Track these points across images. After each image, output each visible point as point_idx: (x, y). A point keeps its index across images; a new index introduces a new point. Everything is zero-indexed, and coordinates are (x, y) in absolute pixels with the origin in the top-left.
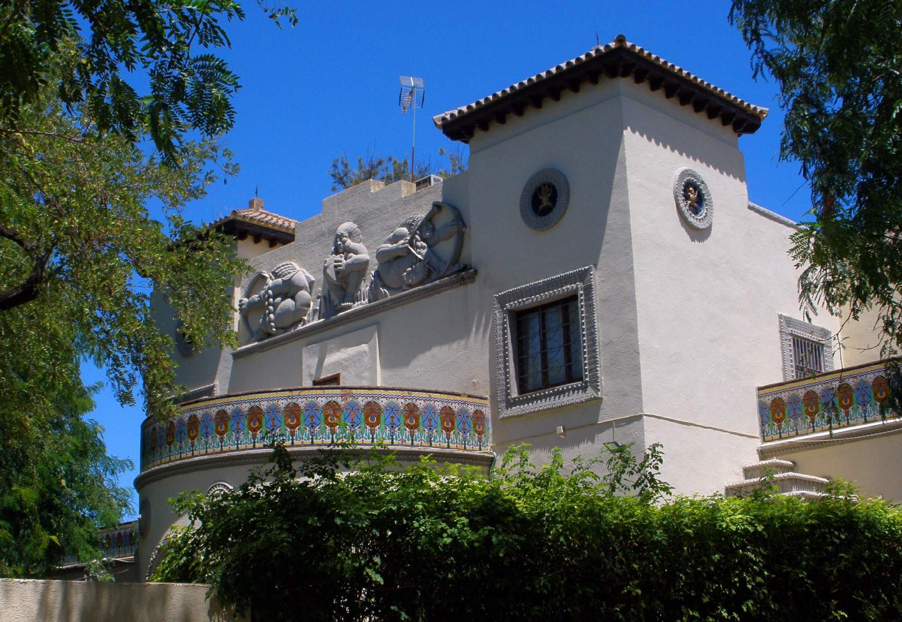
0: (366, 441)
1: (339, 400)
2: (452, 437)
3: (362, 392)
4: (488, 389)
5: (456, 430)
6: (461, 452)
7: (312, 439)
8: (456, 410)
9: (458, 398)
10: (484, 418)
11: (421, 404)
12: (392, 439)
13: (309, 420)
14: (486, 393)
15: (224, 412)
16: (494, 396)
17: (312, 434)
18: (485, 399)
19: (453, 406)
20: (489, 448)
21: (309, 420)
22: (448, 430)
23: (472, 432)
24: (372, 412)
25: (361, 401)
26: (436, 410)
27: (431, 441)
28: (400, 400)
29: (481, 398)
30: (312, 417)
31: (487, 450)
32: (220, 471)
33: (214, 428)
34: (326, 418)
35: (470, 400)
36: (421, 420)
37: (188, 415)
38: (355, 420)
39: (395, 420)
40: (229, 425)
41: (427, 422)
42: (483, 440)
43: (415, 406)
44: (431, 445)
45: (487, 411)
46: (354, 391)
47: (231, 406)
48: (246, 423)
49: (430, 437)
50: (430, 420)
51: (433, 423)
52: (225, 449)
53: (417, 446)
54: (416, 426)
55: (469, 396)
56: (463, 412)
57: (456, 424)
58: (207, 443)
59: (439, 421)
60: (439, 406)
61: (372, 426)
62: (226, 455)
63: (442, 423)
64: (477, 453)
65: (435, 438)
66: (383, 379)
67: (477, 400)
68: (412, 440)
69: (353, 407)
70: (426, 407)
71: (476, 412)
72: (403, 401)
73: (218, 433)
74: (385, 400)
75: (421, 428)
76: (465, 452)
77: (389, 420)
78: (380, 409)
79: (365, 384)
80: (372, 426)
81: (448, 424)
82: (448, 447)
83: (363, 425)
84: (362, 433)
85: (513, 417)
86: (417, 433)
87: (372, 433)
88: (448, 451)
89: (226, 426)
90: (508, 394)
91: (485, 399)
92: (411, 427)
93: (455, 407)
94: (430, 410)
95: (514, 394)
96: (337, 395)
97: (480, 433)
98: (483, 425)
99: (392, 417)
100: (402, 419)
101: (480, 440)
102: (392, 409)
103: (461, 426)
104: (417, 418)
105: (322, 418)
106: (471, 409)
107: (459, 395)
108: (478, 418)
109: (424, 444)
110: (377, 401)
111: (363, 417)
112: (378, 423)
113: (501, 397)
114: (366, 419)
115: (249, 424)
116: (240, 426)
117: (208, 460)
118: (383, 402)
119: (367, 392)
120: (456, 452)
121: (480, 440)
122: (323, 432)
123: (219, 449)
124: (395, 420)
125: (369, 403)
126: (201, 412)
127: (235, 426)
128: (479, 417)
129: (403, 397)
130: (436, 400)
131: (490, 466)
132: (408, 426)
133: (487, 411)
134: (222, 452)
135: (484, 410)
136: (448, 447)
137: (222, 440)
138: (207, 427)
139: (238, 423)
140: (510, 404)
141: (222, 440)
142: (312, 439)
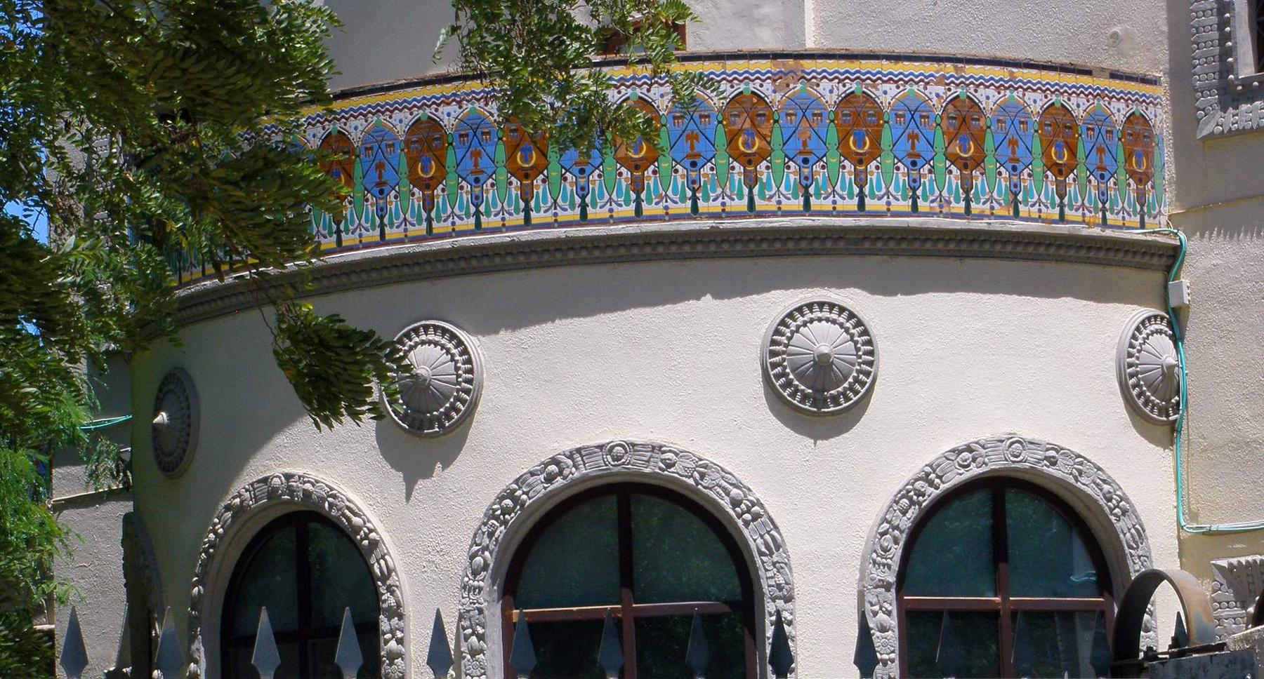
0: (842, 205)
1: (767, 89)
2: (1072, 189)
3: (831, 65)
4: (1163, 54)
5: (1081, 171)
6: (1096, 231)
7: (694, 200)
8: (1079, 113)
9: (1085, 81)
10: (1151, 137)
11: (988, 99)
12: (915, 199)
13: (684, 146)
14: (1155, 64)
15: (434, 124)
16: (1180, 73)
17: (693, 184)
18: (1154, 82)
19: (1072, 104)
20: (1164, 220)
21: (684, 146)
22: (1060, 170)
23: (1122, 176)
24: (859, 123)
25: (829, 93)
26: (1028, 115)
27: (1016, 204)
28: (934, 89)
29: (1144, 80)
30: (692, 137)
31: (1158, 227)
32: (425, 290)
33: (404, 167)
34: (731, 141)
35: (1117, 85)
36: (989, 144)
37: (320, 132)
38: (813, 144)
39: (921, 146)
40: (450, 160)
41: (1006, 150)
42: (1150, 197)
43: (974, 104)
44: (1017, 214)
45: (1161, 119)
46: (808, 65)
47: (453, 108)
48: (501, 153)
49: (1014, 190)
50: (1013, 143)
51: (1020, 151)
52: (438, 227)
53: (981, 216)
54: (977, 162)
55: (1114, 75)
56: (1099, 121)
57: (1081, 154)
58: (381, 212)
59: (1037, 148)
60: (1036, 103)
61: (860, 161)
62: (446, 244)
63: (1046, 153)
64: (1136, 235)
65: (1028, 193)
66: (823, 25)
67: (1133, 87)
68: (968, 201)
69: (806, 109)
70: (1003, 108)
71: (1131, 119)
72: (941, 89)
73: (416, 181)
74: (891, 89)
75: (990, 164)
76: (1109, 233)
77: (904, 145)
78: (879, 113)
79: (768, 40)
80: (860, 161)
81: (1139, 163)
82: (1062, 219)
83: (833, 158)
84: (831, 181)
85: (1242, 132)
86: (978, 181)
87: (860, 181)
88: (1062, 228)
89: (441, 165)
90: (1225, 69)
91: (1154, 82)
92: (964, 165)
93: (1079, 107)
94: (1013, 114)
95: (1246, 67)
96: (760, 76)
97: (1142, 179)
98: (1148, 155)
99: (913, 137)
100: (940, 142)
101: (1141, 198)
102: (914, 113)
103: (904, 145)
104: (979, 140)
105: (721, 140)
106: (1119, 112)
107: (1088, 72)
108: (1136, 137)
109: (998, 211)
110: (872, 92)
111: (833, 136)
112: (875, 152)
113: (1204, 75)
114: (843, 141)
115: (511, 157)
116: (484, 162)
117: (391, 258)
118: (887, 95)
119: (843, 65)
120: (1086, 231)
121: (1141, 198)
122: (722, 179)
123: (421, 229)
124: (921, 146)
125: (848, 98)
126: (360, 122)
127: (469, 163)
128: (1138, 132)
129: (941, 81)
130: (877, 79)
131: (1168, 269)
132: (954, 159)
133: (1161, 119)
134: (430, 235)
135: (1150, 113)
136: (1062, 219)
137: (429, 204)
138: (380, 166)
139: (477, 155)
140: (1232, 96)
141: (429, 204)
142: (694, 200)
